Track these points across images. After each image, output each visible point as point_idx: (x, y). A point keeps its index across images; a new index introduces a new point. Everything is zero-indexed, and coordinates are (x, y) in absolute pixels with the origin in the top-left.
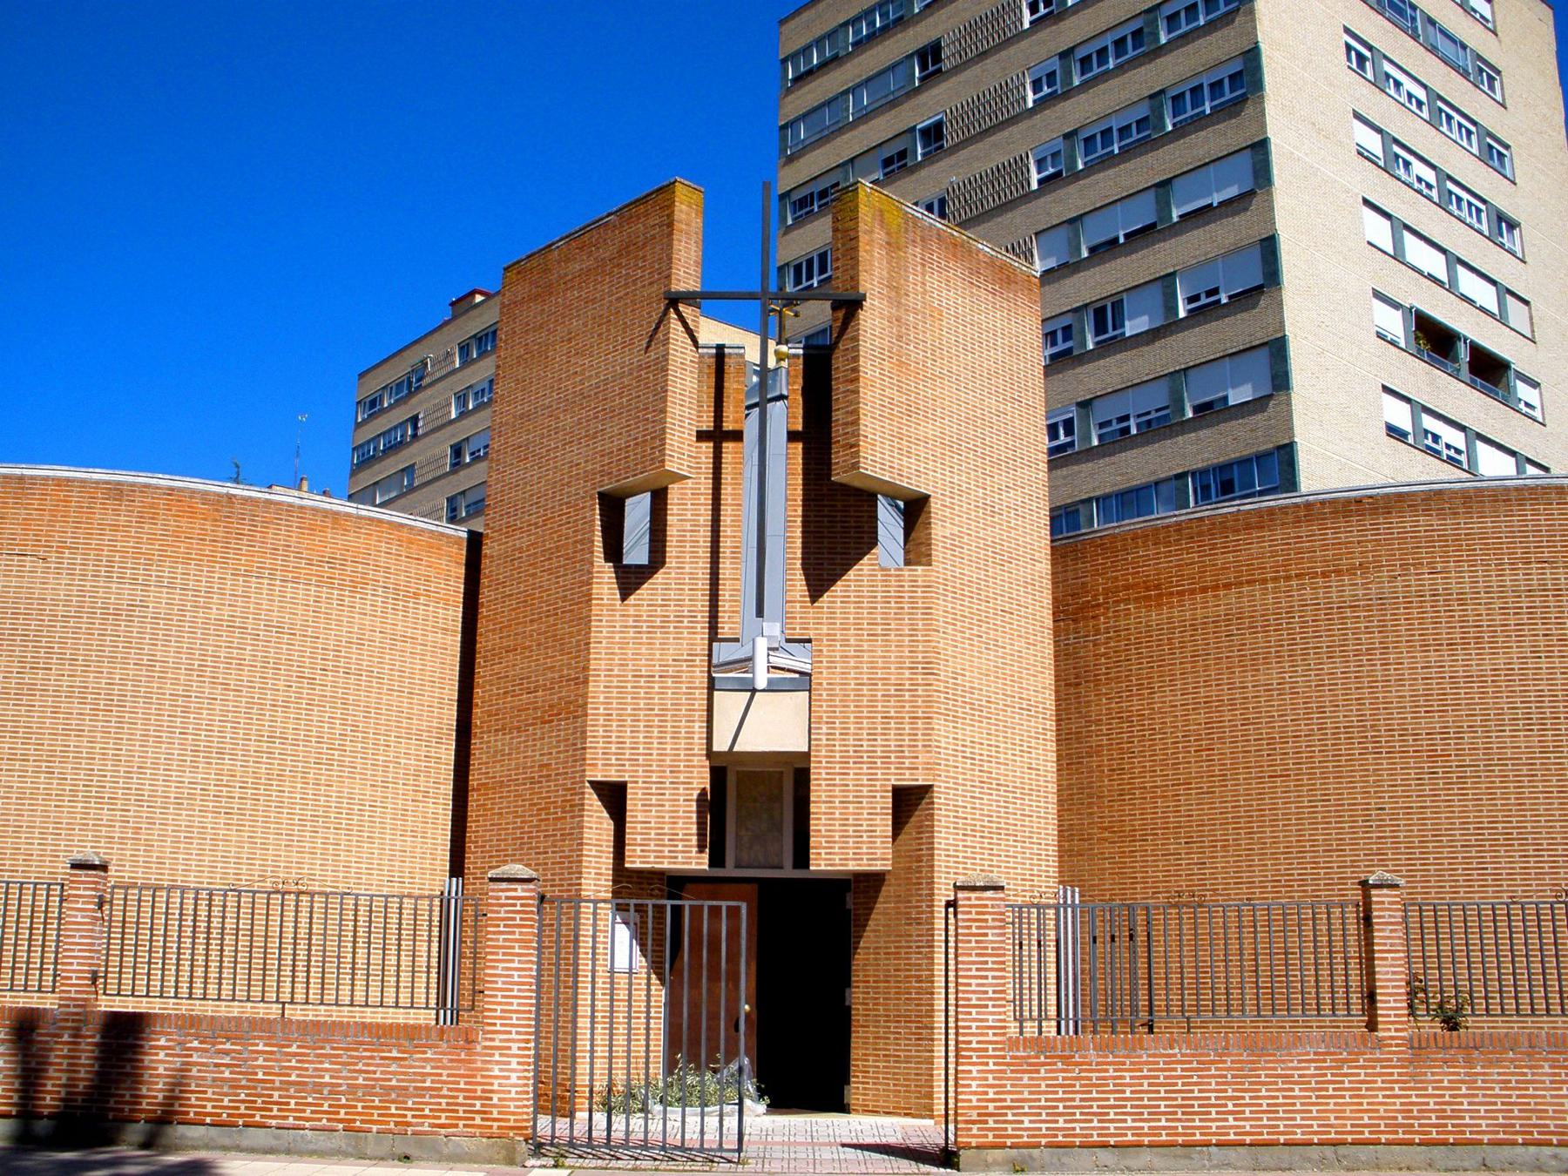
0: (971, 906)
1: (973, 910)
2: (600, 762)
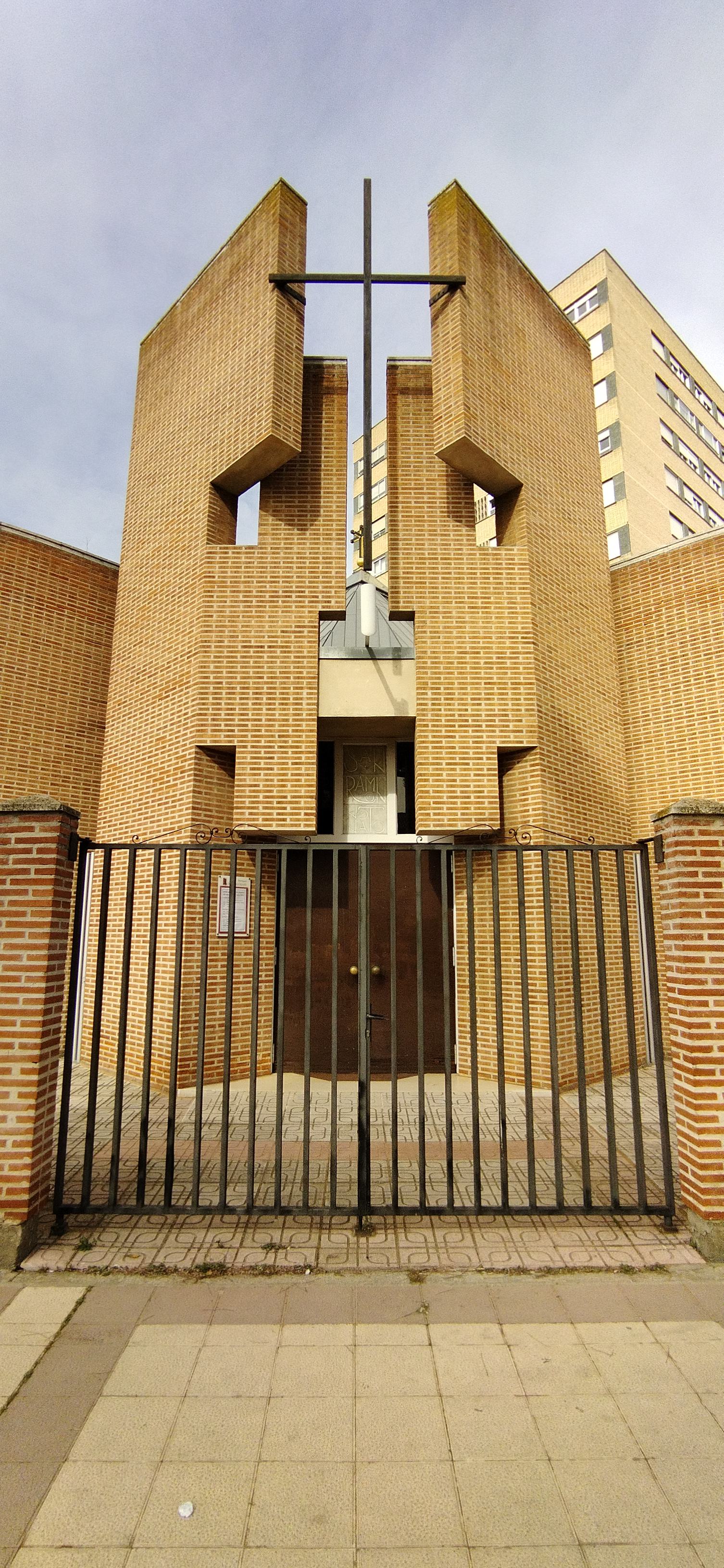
0: (694, 844)
1: (698, 849)
2: (209, 728)
